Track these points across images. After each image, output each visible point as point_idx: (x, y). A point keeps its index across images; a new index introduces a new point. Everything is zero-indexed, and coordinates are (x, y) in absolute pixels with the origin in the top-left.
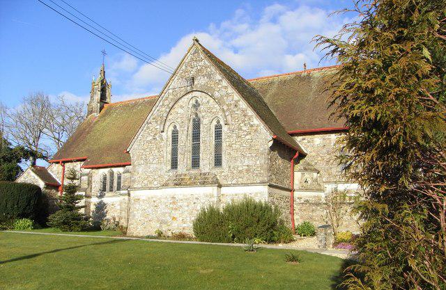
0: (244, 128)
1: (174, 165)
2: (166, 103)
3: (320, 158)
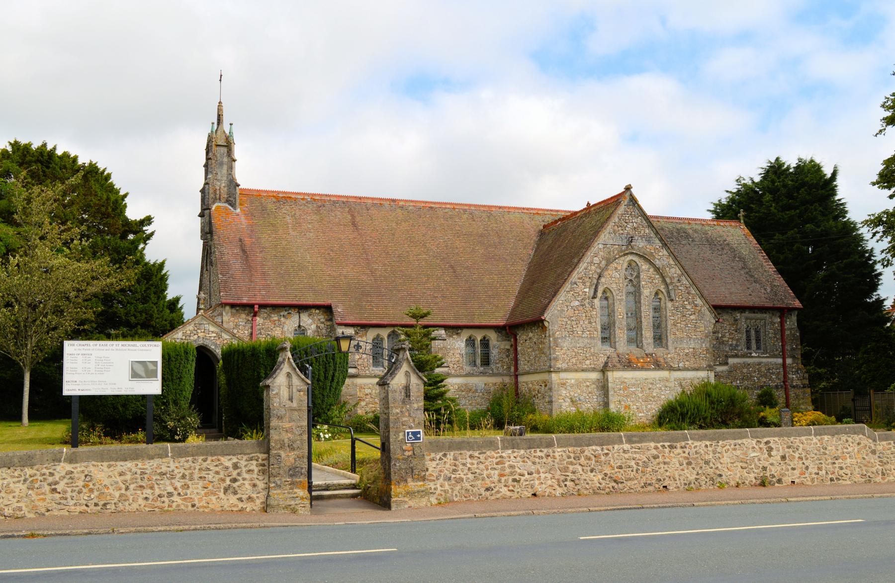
2: (596, 260)
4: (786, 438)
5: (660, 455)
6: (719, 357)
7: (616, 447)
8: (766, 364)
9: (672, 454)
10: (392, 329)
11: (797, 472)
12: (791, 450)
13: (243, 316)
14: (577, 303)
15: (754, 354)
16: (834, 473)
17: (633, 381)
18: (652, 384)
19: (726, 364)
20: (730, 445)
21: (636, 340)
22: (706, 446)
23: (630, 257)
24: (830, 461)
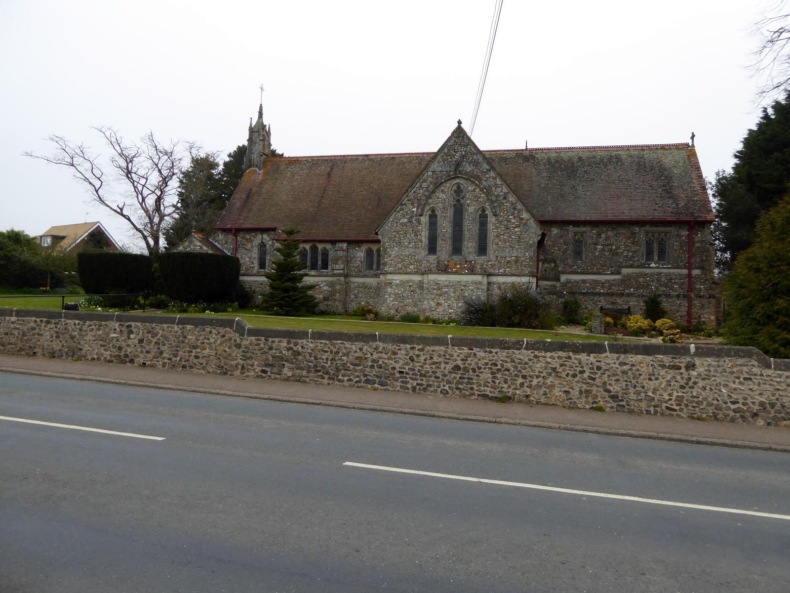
0: (513, 221)
1: (432, 249)
2: (425, 185)
3: (556, 248)
4: (148, 324)
5: (37, 328)
6: (612, 267)
7: (7, 318)
8: (667, 275)
9: (47, 329)
10: (313, 243)
11: (150, 356)
12: (150, 335)
13: (230, 236)
14: (406, 220)
15: (653, 265)
16: (188, 361)
17: (447, 283)
18: (464, 286)
19: (619, 273)
20: (95, 325)
21: (457, 249)
22: (75, 324)
23: (457, 181)
24: (188, 349)
